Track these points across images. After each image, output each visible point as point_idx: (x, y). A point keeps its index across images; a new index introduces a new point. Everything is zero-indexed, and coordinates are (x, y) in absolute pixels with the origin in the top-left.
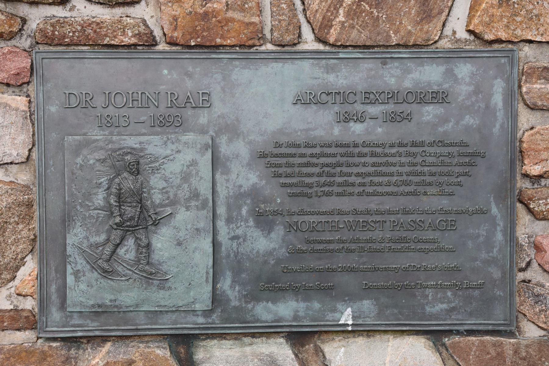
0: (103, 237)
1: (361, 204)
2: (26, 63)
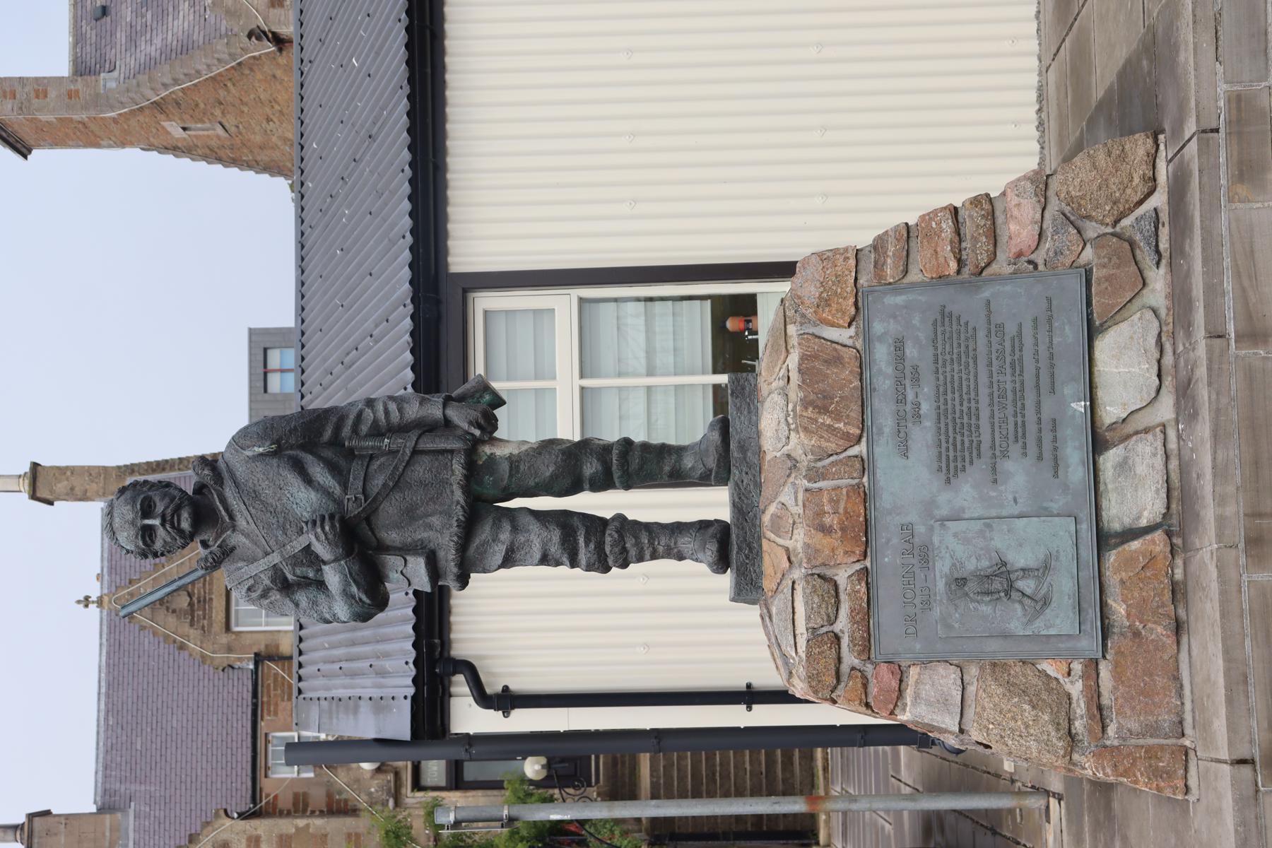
0: (1018, 606)
2: (884, 667)
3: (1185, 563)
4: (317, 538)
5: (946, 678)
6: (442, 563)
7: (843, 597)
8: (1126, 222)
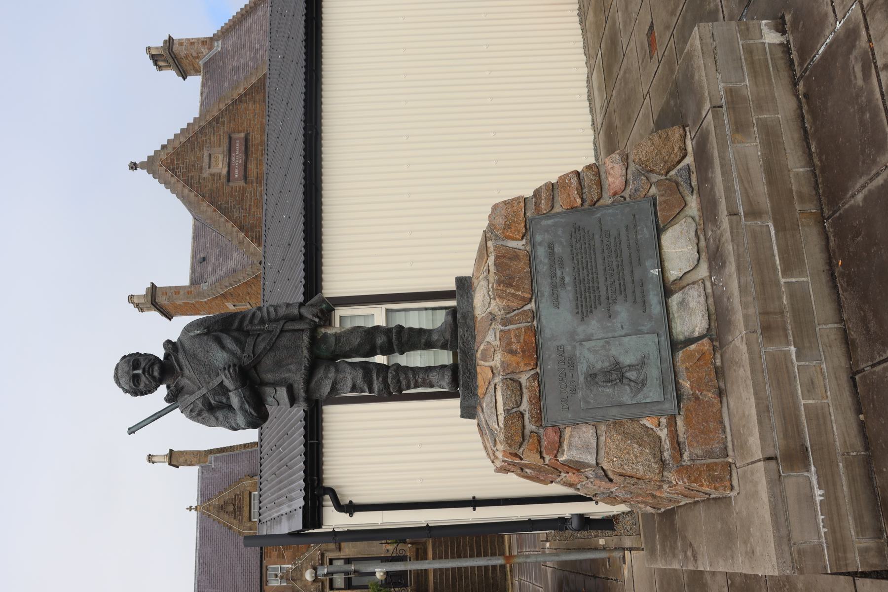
0: (627, 387)
1: (601, 272)
2: (550, 429)
3: (721, 356)
4: (226, 376)
5: (587, 433)
6: (296, 391)
7: (524, 390)
8: (672, 173)
